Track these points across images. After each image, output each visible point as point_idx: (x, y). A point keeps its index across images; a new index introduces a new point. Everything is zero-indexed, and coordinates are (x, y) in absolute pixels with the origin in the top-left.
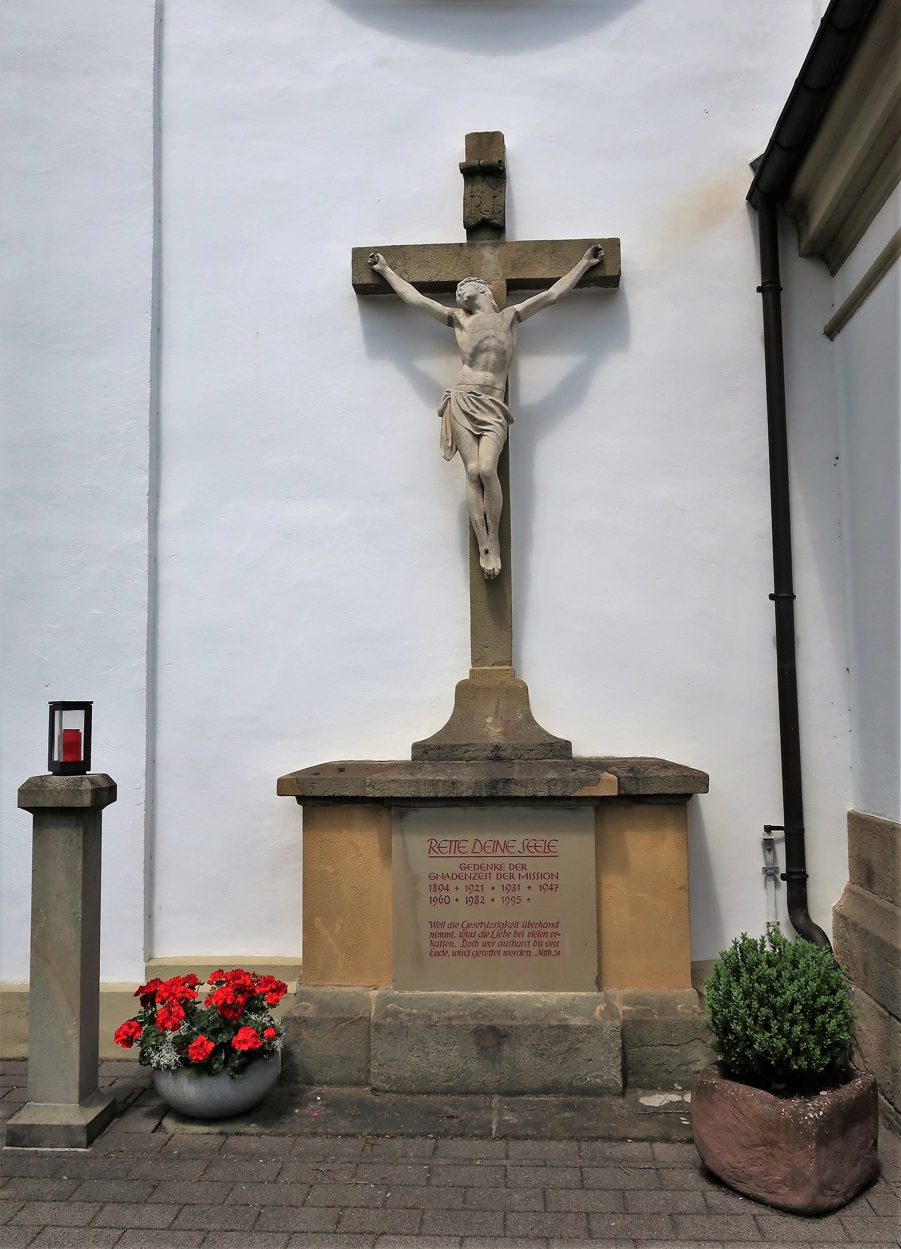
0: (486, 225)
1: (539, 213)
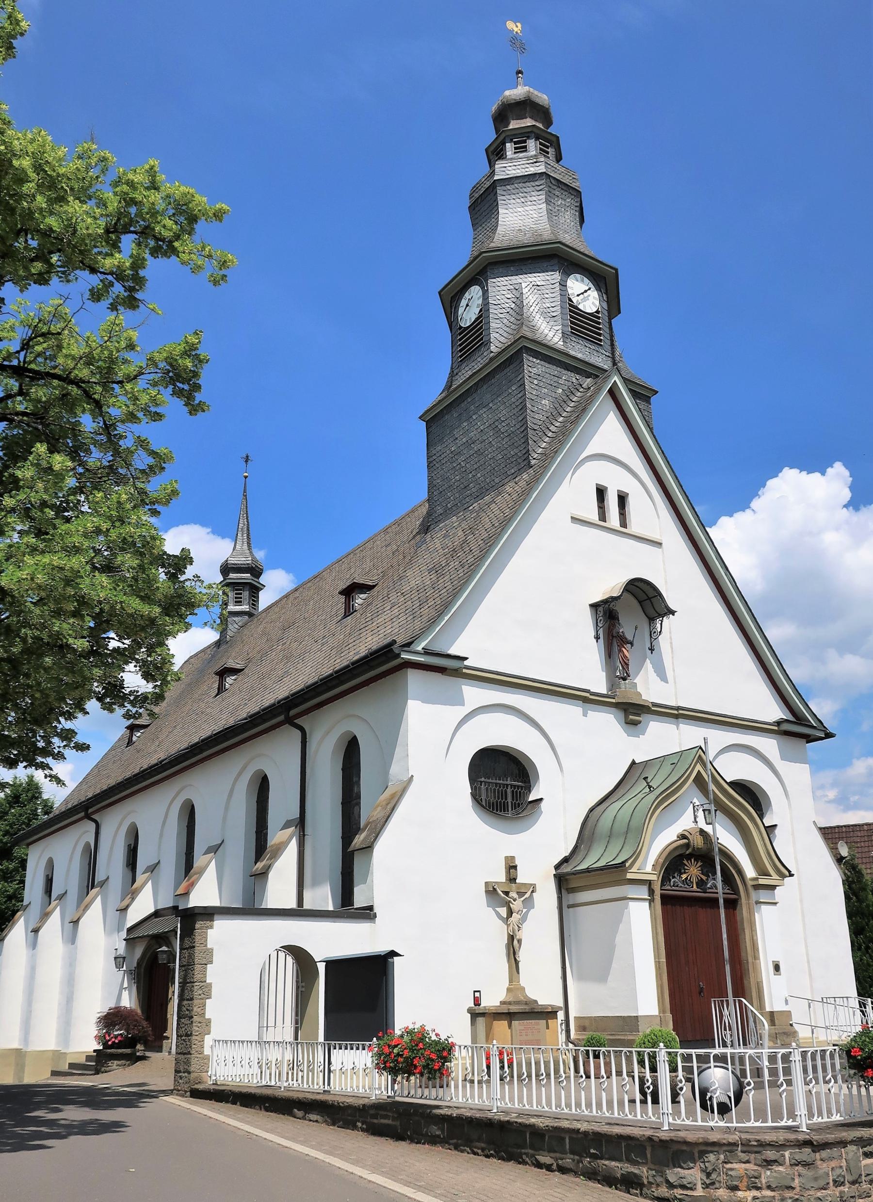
0: (512, 880)
1: (522, 878)
